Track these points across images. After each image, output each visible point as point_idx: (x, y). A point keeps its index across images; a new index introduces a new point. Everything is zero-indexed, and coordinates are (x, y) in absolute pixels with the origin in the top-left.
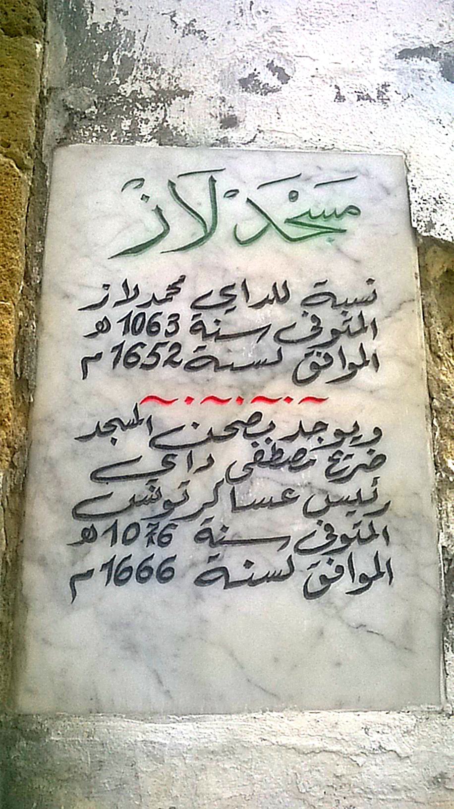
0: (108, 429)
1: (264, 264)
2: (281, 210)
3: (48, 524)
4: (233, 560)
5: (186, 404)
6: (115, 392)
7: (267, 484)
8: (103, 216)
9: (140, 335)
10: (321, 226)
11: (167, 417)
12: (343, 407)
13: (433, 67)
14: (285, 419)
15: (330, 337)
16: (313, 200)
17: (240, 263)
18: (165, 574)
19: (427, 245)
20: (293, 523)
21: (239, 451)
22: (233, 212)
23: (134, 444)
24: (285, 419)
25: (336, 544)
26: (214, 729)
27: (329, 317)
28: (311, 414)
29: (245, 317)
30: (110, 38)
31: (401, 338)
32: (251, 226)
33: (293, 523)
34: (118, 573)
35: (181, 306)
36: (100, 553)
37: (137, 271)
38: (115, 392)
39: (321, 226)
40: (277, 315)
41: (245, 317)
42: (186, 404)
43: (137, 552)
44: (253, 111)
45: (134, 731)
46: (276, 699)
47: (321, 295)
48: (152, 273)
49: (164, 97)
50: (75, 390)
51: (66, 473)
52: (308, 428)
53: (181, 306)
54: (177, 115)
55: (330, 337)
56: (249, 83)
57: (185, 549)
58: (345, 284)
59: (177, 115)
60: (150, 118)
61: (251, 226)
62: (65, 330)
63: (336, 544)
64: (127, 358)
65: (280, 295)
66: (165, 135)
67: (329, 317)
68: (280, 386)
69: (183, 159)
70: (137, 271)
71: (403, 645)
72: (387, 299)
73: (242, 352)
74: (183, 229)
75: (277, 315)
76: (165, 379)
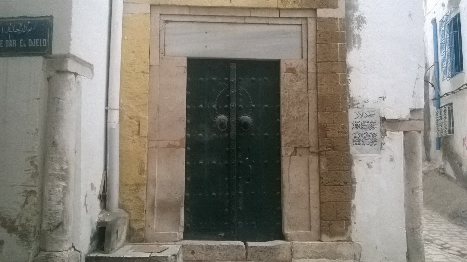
0: (354, 134)
1: (367, 119)
2: (368, 114)
3: (351, 141)
4: (365, 143)
5: (361, 131)
6: (355, 130)
7: (367, 138)
8: (353, 115)
9: (357, 126)
10: (371, 116)
11: (359, 132)
12: (373, 131)
13: (446, 133)
14: (369, 132)
15: (372, 125)
16: (371, 113)
17: (365, 119)
18: (360, 144)
19: (381, 117)
20: (369, 141)
21: (365, 135)
22: (364, 115)
23: (357, 135)
24: (369, 132)
25: (373, 142)
26: (364, 155)
27: (372, 124)
28: (371, 132)
29: (365, 124)
30: (352, 98)
31: (378, 126)
32: (366, 116)
33: (369, 141)
34: (356, 144)
35: (360, 123)
36: (355, 143)
37: (356, 120)
38: (355, 130)
39: (371, 116)
40: (368, 124)
41: (365, 124)
42: (361, 131)
43: (357, 143)
44: (365, 104)
45: (357, 155)
46: (368, 153)
47: (372, 122)
48: (357, 120)
49: (358, 104)
50: (352, 130)
51: (351, 137)
52: (136, 71)
53: (360, 123)
54: (359, 105)
55: (372, 125)
56: (365, 102)
57: (361, 142)
58: (374, 121)
59: (359, 105)
60: (356, 106)
61: (366, 116)
62: (351, 125)
63: (373, 142)
64: (356, 128)
65: (368, 122)
66: (358, 108)
67: (372, 124)
68: (368, 130)
69: (359, 110)
70: (356, 120)
71: (378, 149)
72: (377, 122)
73: (365, 127)
74: (360, 116)
75: (368, 124)
76: (359, 129)
